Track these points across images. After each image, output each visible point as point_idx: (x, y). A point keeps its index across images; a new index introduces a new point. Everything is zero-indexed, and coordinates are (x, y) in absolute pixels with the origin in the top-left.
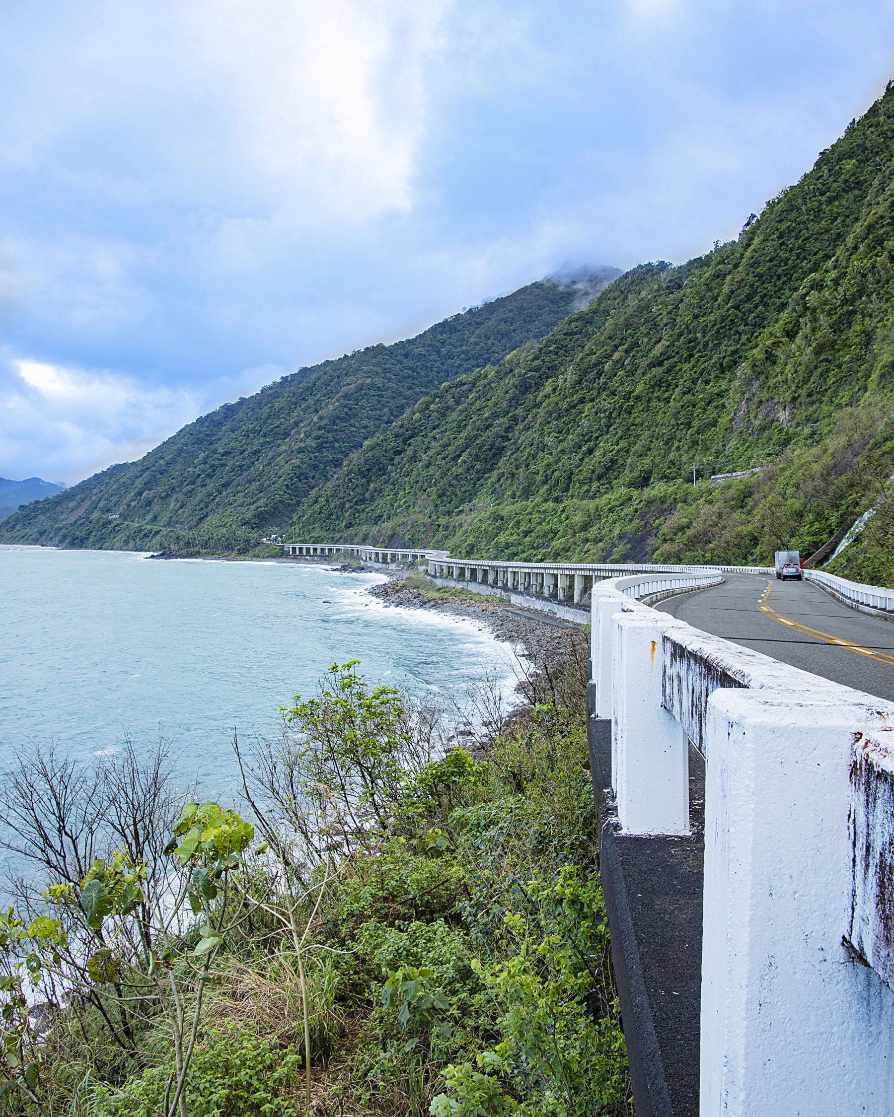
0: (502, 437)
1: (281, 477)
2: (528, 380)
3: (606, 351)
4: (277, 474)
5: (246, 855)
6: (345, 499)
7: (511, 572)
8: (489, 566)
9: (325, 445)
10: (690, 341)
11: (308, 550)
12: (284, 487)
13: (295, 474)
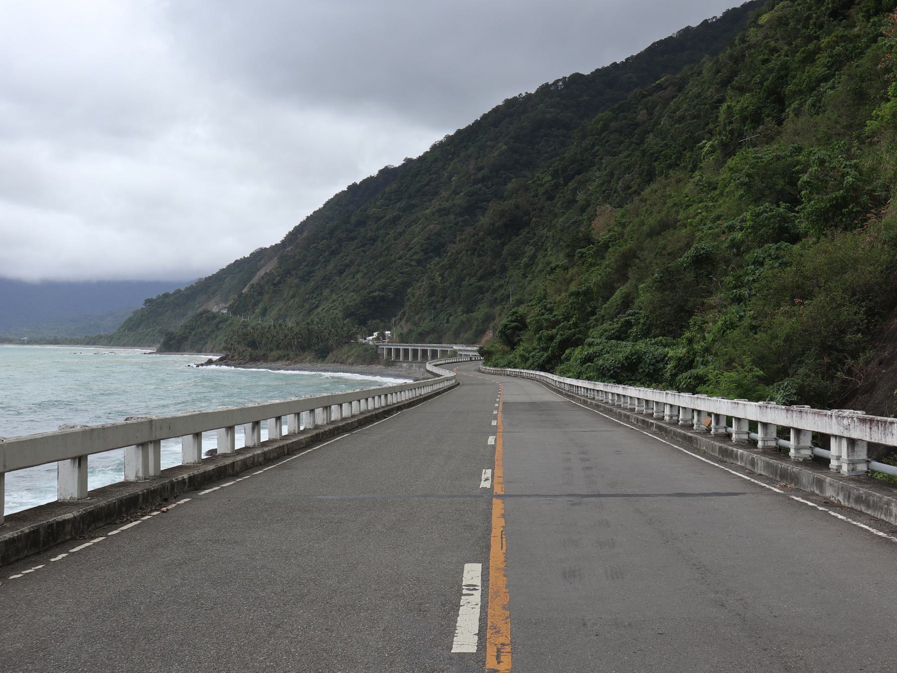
11: (406, 351)
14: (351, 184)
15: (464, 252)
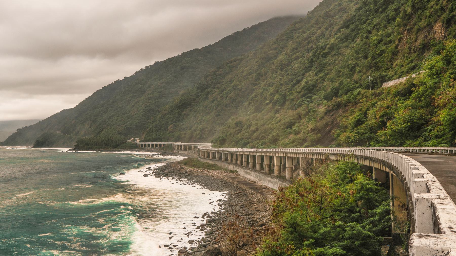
0: (253, 84)
1: (139, 111)
2: (269, 55)
3: (313, 30)
4: (137, 110)
5: (436, 101)
6: (169, 120)
7: (240, 154)
8: (228, 151)
9: (163, 95)
10: (367, 11)
11: (149, 145)
12: (141, 116)
13: (147, 109)
15: (167, 114)
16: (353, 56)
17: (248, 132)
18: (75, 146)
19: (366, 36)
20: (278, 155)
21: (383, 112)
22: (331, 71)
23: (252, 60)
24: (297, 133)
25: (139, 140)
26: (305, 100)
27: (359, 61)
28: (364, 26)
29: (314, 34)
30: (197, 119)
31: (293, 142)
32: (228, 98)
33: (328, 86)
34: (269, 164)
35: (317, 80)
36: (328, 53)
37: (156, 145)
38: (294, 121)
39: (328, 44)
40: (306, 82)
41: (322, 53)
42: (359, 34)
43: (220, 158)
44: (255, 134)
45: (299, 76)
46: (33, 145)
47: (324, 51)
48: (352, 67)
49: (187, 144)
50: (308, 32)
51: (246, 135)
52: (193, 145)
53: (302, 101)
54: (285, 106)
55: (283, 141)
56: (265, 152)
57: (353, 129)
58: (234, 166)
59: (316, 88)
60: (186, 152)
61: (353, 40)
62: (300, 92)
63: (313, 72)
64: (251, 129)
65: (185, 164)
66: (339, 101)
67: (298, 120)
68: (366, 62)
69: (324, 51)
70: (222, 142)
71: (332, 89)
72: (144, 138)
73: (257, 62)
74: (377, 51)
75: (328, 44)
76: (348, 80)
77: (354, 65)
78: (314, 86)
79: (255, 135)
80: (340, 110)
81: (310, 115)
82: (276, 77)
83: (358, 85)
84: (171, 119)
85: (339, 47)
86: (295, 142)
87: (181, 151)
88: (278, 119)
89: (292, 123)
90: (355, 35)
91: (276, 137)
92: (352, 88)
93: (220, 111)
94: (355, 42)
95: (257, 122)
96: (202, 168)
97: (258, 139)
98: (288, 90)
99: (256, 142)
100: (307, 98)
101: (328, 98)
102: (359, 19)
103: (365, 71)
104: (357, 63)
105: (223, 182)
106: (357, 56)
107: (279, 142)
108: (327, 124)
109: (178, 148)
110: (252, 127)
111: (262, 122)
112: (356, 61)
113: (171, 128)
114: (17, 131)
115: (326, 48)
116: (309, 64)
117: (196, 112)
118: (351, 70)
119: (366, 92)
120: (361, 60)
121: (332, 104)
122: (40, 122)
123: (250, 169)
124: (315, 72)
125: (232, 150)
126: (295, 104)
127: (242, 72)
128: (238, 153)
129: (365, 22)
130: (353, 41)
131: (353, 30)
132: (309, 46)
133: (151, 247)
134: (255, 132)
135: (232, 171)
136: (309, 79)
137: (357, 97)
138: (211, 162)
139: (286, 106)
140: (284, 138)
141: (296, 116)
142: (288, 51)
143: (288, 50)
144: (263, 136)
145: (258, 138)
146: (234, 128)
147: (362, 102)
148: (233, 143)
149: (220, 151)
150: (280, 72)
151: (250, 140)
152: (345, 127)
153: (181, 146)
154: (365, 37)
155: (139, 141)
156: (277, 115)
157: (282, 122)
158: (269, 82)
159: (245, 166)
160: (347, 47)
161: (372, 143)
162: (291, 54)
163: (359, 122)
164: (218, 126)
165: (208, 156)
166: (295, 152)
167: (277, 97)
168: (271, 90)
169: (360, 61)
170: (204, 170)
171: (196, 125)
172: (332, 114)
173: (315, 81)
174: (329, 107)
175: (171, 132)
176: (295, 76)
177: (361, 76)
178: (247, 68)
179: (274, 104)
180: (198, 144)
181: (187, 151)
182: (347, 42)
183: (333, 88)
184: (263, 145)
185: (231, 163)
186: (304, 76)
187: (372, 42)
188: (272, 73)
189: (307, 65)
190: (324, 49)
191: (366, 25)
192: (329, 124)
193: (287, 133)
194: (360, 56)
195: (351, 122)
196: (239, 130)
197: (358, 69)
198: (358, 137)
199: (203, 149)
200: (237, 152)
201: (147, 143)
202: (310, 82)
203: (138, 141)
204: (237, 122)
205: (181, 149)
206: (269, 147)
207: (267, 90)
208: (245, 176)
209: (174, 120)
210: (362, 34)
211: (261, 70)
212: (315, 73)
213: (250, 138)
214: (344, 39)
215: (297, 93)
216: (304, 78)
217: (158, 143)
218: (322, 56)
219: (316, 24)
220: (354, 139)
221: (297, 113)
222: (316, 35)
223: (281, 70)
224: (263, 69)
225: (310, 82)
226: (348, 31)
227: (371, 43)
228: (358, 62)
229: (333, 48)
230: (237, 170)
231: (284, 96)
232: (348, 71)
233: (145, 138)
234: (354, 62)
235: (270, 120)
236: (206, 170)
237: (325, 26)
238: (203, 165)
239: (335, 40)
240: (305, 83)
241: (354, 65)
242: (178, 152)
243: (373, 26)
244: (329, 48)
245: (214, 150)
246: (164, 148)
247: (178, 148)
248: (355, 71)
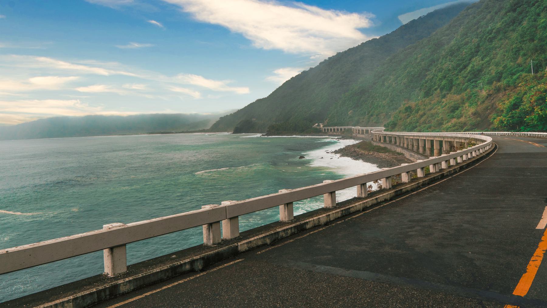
3: (483, 15)
7: (406, 138)
8: (397, 135)
11: (331, 129)
14: (291, 77)
15: (347, 100)
16: (517, 40)
17: (416, 116)
18: (267, 131)
19: (534, 19)
20: (437, 139)
21: (538, 96)
22: (497, 55)
23: (426, 47)
24: (459, 117)
25: (323, 125)
26: (471, 85)
27: (524, 45)
28: (533, 9)
29: (484, 19)
30: (374, 105)
31: (454, 126)
32: (402, 84)
33: (493, 70)
34: (439, 148)
35: (483, 65)
36: (494, 38)
37: (334, 129)
38: (458, 105)
39: (494, 29)
40: (472, 67)
41: (488, 38)
42: (526, 16)
43: (390, 141)
44: (423, 118)
45: (466, 62)
46: (233, 131)
47: (490, 36)
48: (516, 51)
49: (364, 128)
50: (478, 17)
51: (414, 120)
52: (369, 129)
53: (468, 86)
54: (452, 91)
55: (447, 125)
56: (426, 137)
57: (507, 113)
58: (402, 149)
59: (482, 73)
60: (364, 135)
61: (520, 24)
62: (466, 77)
63: (479, 57)
64: (419, 113)
65: (358, 148)
66: (499, 86)
67: (462, 104)
68: (532, 45)
69: (490, 36)
70: (392, 126)
71: (496, 73)
72: (326, 123)
73: (430, 48)
74: (545, 34)
75: (494, 29)
76: (512, 64)
77: (518, 49)
78: (480, 71)
79: (423, 119)
80: (501, 94)
81: (472, 99)
82: (446, 63)
83: (521, 68)
84: (351, 105)
85: (505, 31)
86: (457, 126)
87: (359, 135)
88: (444, 104)
89: (456, 108)
90: (522, 18)
91: (440, 121)
92: (515, 72)
93: (395, 96)
94: (522, 25)
95: (425, 106)
96: (372, 151)
97: (425, 123)
98: (454, 75)
99: (422, 126)
100: (472, 83)
101: (490, 83)
102: (527, 2)
103: (530, 54)
104: (521, 46)
105: (388, 164)
106: (522, 39)
107: (443, 125)
108: (487, 109)
109: (356, 132)
110: (420, 112)
111: (429, 107)
112: (521, 45)
113: (351, 113)
114: (220, 119)
115: (493, 33)
116: (476, 49)
117: (373, 98)
118: (516, 54)
119: (526, 76)
120: (526, 43)
121: (493, 89)
122: (221, 118)
123: (414, 152)
124: (482, 56)
125: (399, 134)
126: (461, 89)
127: (416, 59)
128: (405, 137)
129: (534, 5)
130: (520, 24)
131: (520, 13)
132: (478, 31)
133: (208, 213)
134: (422, 116)
135: (399, 154)
136: (475, 64)
137: (516, 82)
138: (382, 145)
139: (453, 91)
140: (448, 122)
141: (460, 101)
142: (459, 37)
143: (458, 36)
144: (430, 120)
145: (425, 122)
146: (404, 113)
147: (521, 87)
148: (403, 127)
149: (390, 135)
150: (449, 58)
151: (418, 124)
152: (502, 111)
153: (359, 130)
154: (532, 19)
155: (322, 125)
156: (444, 100)
157: (448, 106)
158: (439, 68)
159: (411, 149)
160: (514, 30)
161: (522, 128)
162: (460, 39)
163: (515, 106)
164: (393, 111)
165: (380, 140)
166: (450, 137)
167: (445, 83)
168: (440, 75)
169: (525, 44)
170: (374, 153)
171: (373, 110)
172: (492, 98)
173: (480, 66)
174: (490, 91)
175: (351, 117)
176: (462, 61)
177: (525, 60)
178: (421, 55)
179: (442, 89)
180: (374, 128)
181: (364, 134)
182: (513, 25)
183: (497, 72)
184: (429, 129)
185: (399, 146)
186: (471, 61)
187: (540, 24)
188: (443, 59)
189: (474, 50)
190: (491, 34)
191: (535, 7)
192: (489, 108)
193: (450, 117)
194: (525, 39)
195: (506, 106)
196: (409, 115)
197: (522, 53)
198: (511, 122)
199: (376, 133)
200: (404, 136)
201: (329, 128)
202: (475, 67)
203: (322, 126)
204: (406, 107)
205: (359, 133)
206: (432, 131)
207: (437, 76)
208: (410, 159)
209: (353, 106)
210: (529, 17)
211: (433, 56)
212: (481, 57)
213: (418, 122)
214: (511, 23)
215: (464, 78)
216: (471, 63)
217: (339, 128)
218: (488, 41)
219: (485, 9)
220: (507, 124)
221: (461, 98)
222: (485, 20)
223: (451, 55)
224: (436, 55)
225: (475, 67)
226: (515, 15)
227: (539, 26)
228: (523, 46)
229: (499, 33)
230: (404, 153)
231: (451, 81)
232: (512, 55)
233: (328, 123)
234: (518, 45)
235: (436, 105)
236: (376, 153)
237: (495, 11)
238: (374, 148)
239: (501, 25)
240: (471, 68)
241: (518, 49)
242: (356, 135)
243: (542, 8)
244: (495, 33)
245: (385, 134)
246: (344, 132)
247: (356, 132)
248: (519, 54)
